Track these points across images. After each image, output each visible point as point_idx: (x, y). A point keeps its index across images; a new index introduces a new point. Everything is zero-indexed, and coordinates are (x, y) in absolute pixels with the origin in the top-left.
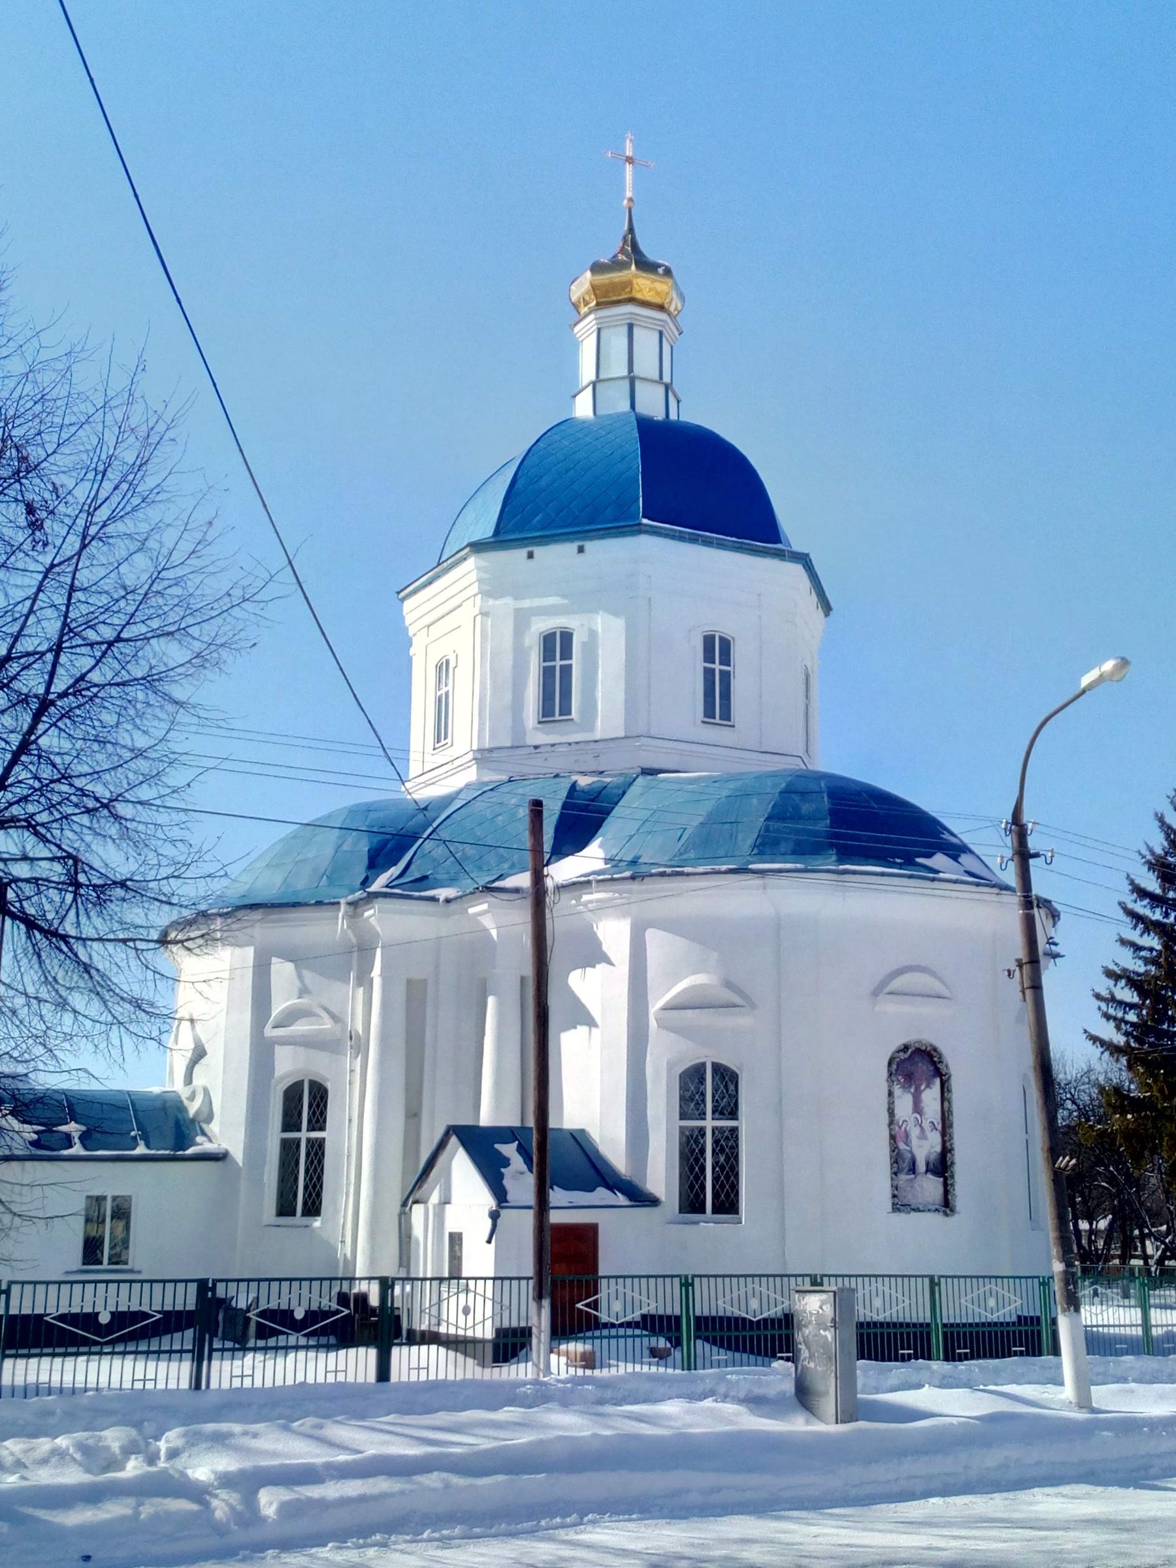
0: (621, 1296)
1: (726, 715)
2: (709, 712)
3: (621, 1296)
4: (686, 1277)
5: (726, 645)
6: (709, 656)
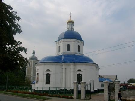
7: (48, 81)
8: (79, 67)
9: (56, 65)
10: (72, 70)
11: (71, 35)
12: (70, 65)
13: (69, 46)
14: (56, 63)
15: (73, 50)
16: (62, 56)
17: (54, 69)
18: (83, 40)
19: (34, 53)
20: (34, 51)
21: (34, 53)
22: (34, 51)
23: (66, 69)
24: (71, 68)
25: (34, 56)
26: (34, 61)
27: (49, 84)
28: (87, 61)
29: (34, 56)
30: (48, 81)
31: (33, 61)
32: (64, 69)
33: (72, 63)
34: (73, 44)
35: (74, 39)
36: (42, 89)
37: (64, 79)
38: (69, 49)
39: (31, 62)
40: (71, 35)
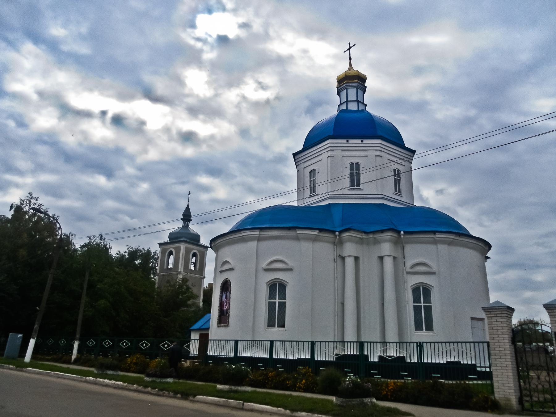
0: (338, 348)
1: (358, 185)
2: (352, 185)
3: (338, 348)
4: (420, 343)
5: (358, 165)
6: (352, 169)
7: (276, 317)
8: (417, 252)
9: (315, 239)
10: (388, 263)
11: (353, 122)
12: (377, 242)
13: (355, 167)
14: (315, 233)
15: (375, 189)
16: (30, 365)
17: (303, 257)
18: (407, 145)
19: (187, 217)
20: (188, 208)
21: (187, 217)
22: (188, 208)
23: (357, 259)
24: (381, 258)
25: (186, 227)
26: (187, 248)
27: (416, 330)
28: (438, 226)
29: (186, 227)
30: (276, 317)
31: (183, 247)
32: (350, 263)
33: (388, 235)
34: (370, 153)
35: (379, 141)
36: (266, 355)
37: (333, 309)
38: (355, 182)
39: (178, 250)
40: (353, 122)
